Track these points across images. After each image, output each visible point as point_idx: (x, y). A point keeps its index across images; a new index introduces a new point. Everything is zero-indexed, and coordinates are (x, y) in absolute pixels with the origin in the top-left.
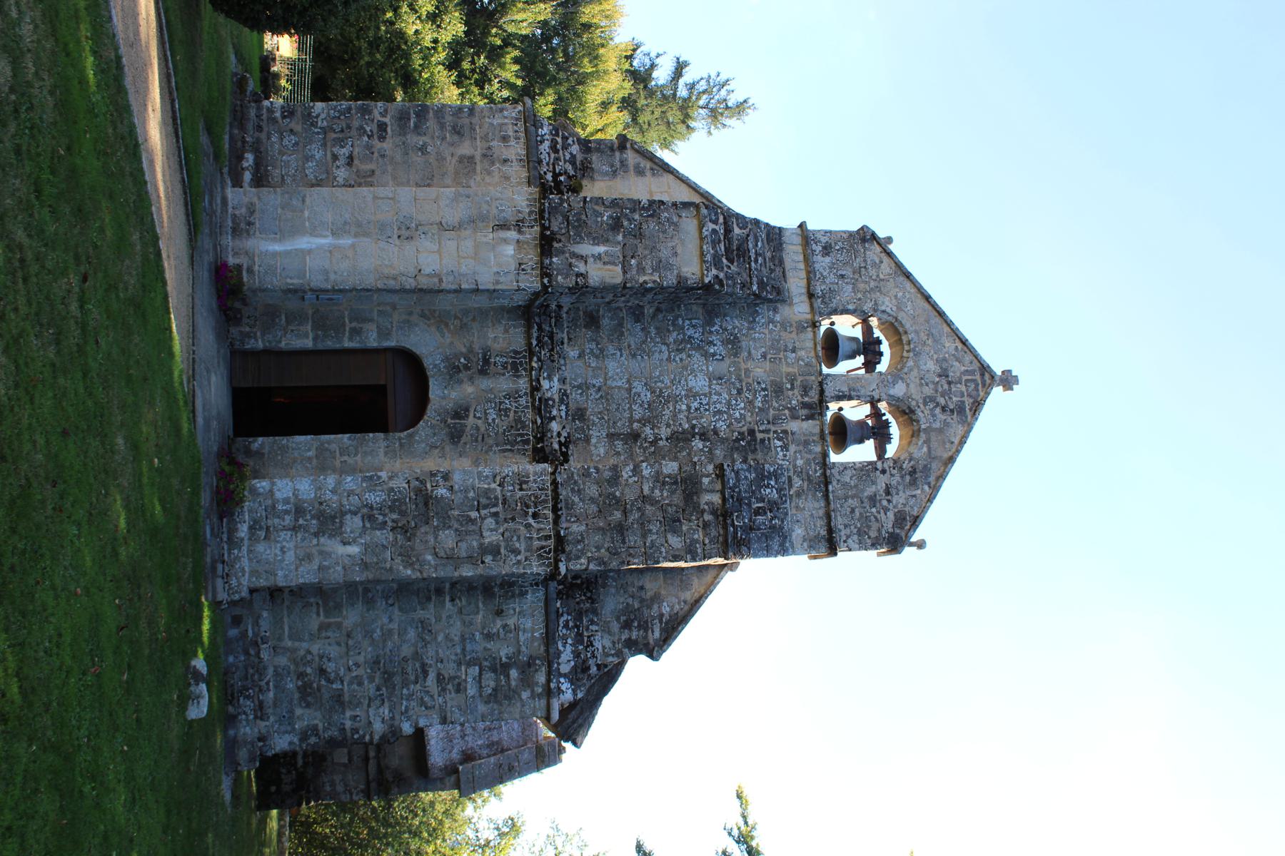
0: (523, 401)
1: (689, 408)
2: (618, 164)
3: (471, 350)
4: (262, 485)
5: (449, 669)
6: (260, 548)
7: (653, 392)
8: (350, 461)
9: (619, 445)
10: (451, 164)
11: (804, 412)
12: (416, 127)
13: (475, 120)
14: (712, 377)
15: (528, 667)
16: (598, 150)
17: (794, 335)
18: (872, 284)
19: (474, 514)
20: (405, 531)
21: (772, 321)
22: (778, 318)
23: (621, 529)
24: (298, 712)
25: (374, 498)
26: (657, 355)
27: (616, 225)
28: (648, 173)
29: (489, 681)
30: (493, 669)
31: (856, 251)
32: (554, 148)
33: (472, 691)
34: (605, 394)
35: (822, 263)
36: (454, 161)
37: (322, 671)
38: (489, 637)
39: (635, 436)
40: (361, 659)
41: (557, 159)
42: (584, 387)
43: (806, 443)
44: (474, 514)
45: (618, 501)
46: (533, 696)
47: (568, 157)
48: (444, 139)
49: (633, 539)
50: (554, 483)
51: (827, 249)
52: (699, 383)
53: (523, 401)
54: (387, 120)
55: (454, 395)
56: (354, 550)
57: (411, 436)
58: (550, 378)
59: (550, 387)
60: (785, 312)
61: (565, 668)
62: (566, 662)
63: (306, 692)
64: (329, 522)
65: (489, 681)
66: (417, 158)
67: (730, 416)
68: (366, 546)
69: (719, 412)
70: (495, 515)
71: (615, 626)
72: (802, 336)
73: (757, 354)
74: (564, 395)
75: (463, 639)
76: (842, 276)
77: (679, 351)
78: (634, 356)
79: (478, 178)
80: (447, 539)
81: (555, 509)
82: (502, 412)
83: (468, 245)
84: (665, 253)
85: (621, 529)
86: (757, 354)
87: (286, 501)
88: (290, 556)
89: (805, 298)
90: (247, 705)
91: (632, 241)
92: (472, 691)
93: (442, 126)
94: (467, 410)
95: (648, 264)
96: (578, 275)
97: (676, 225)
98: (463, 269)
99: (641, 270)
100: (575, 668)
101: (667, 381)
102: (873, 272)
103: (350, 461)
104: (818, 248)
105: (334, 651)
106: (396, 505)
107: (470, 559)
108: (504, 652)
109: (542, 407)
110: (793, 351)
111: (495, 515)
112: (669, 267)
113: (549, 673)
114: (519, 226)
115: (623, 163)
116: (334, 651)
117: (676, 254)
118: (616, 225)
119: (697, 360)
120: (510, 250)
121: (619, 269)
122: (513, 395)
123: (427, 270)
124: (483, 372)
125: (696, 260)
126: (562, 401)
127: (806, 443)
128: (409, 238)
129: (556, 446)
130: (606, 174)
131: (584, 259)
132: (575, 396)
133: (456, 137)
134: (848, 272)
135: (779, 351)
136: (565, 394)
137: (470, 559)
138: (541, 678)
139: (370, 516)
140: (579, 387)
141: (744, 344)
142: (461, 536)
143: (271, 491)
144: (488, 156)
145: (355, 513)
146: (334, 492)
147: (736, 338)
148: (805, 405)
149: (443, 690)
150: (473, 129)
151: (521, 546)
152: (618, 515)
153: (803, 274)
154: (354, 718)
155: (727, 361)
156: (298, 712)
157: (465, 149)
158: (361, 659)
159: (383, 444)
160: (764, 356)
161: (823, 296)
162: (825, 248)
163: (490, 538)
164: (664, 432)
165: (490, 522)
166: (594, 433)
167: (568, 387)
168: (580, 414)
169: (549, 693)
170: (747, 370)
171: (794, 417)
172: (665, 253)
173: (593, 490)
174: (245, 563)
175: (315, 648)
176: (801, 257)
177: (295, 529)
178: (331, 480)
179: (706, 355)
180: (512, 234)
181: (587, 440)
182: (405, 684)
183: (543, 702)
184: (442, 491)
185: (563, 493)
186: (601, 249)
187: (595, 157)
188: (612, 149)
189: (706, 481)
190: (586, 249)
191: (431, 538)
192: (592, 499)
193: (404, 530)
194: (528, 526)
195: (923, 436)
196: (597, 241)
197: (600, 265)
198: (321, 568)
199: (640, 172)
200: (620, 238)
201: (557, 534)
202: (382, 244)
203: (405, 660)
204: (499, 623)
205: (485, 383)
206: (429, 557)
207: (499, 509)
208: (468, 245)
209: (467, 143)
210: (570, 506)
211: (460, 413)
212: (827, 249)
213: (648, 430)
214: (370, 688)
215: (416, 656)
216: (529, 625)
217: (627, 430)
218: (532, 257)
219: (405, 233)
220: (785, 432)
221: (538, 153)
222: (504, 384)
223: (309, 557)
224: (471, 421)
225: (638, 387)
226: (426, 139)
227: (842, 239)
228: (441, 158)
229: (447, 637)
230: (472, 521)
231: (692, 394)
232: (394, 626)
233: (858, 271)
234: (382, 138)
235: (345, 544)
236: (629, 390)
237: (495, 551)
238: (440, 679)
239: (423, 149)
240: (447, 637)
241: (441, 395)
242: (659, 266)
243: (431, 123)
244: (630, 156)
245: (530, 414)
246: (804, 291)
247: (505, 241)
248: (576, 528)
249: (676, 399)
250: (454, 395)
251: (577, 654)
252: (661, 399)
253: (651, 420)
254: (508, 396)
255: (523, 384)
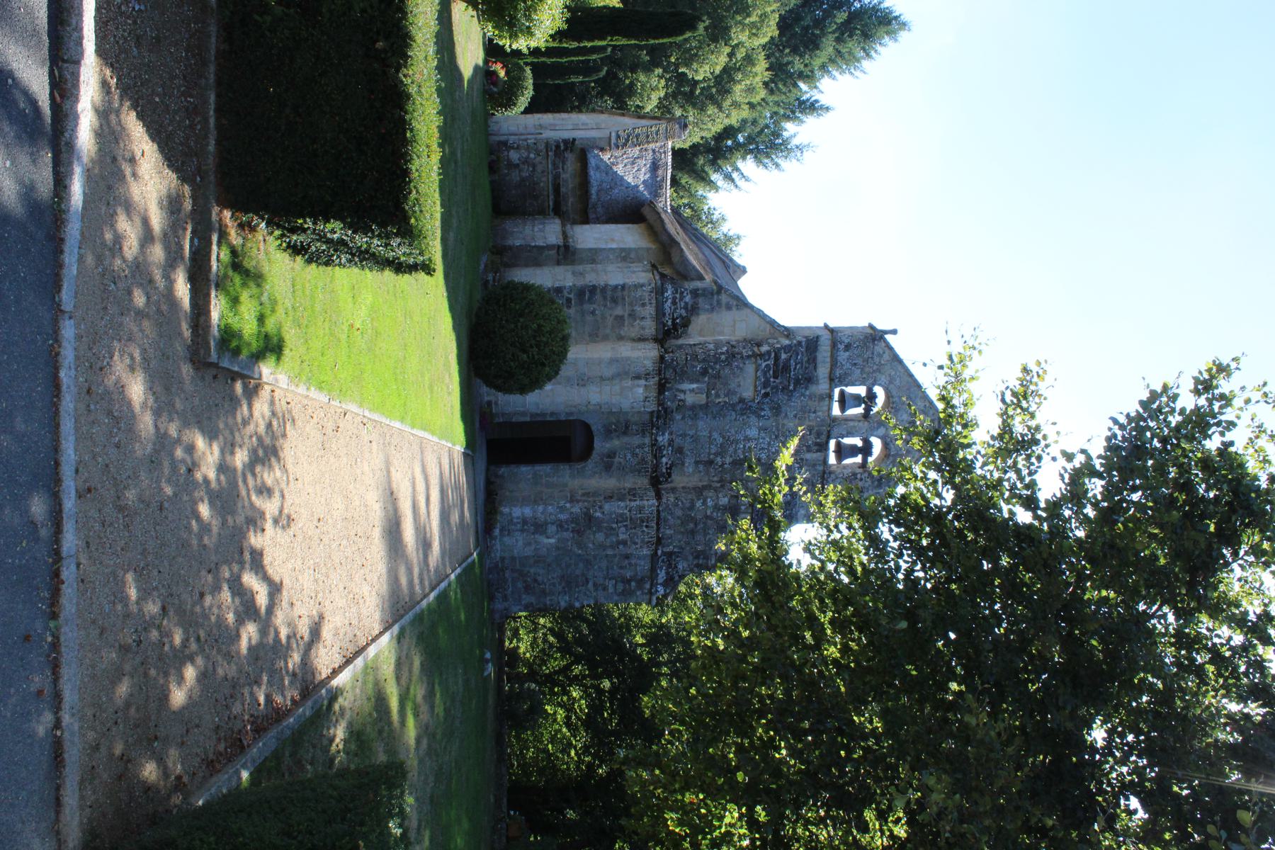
0: (646, 449)
1: (744, 446)
2: (715, 303)
3: (618, 421)
4: (506, 510)
5: (600, 581)
6: (506, 539)
7: (724, 438)
8: (551, 480)
9: (701, 467)
10: (610, 321)
11: (816, 448)
12: (589, 299)
13: (626, 293)
14: (760, 429)
15: (640, 582)
16: (704, 295)
17: (816, 403)
18: (875, 367)
19: (614, 526)
20: (578, 532)
21: (803, 395)
22: (807, 393)
23: (693, 532)
24: (524, 596)
25: (563, 517)
26: (728, 418)
27: (704, 372)
28: (734, 309)
29: (620, 587)
30: (623, 582)
31: (868, 348)
32: (674, 303)
33: (611, 590)
34: (695, 439)
35: (843, 356)
36: (612, 319)
37: (535, 580)
38: (621, 568)
39: (711, 462)
40: (555, 576)
41: (676, 309)
42: (684, 435)
43: (814, 465)
44: (614, 526)
45: (692, 518)
46: (643, 594)
47: (683, 304)
48: (605, 306)
49: (699, 537)
50: (658, 511)
51: (848, 347)
52: (753, 433)
53: (646, 449)
54: (572, 296)
55: (608, 445)
56: (552, 541)
57: (584, 467)
58: (663, 434)
59: (663, 439)
60: (813, 389)
61: (660, 580)
62: (662, 575)
63: (527, 588)
64: (539, 527)
65: (620, 587)
66: (589, 318)
67: (769, 450)
68: (559, 539)
69: (763, 449)
70: (626, 526)
71: (691, 558)
72: (822, 403)
73: (791, 415)
74: (671, 442)
75: (608, 569)
76: (855, 364)
77: (742, 414)
78: (715, 418)
79: (626, 329)
80: (600, 537)
81: (658, 524)
82: (634, 455)
83: (617, 388)
84: (733, 386)
85: (693, 532)
86: (791, 415)
87: (518, 518)
88: (520, 543)
89: (827, 380)
90: (499, 595)
91: (713, 380)
92: (611, 590)
93: (605, 298)
94: (615, 454)
95: (722, 393)
96: (680, 400)
97: (741, 369)
98: (614, 401)
99: (717, 396)
100: (666, 581)
101: (733, 432)
102: (877, 360)
103: (551, 480)
104: (841, 347)
105: (541, 572)
106: (574, 520)
107: (612, 547)
108: (628, 574)
109: (657, 451)
110: (815, 412)
111: (626, 526)
112: (735, 393)
113: (652, 585)
114: (647, 376)
115: (719, 302)
116: (541, 572)
117: (739, 386)
118: (704, 372)
119: (753, 419)
120: (641, 390)
121: (704, 395)
122: (641, 446)
123: (593, 402)
124: (625, 433)
125: (752, 388)
126: (669, 445)
127: (814, 465)
128: (584, 385)
129: (664, 471)
130: (708, 310)
131: (684, 392)
132: (678, 441)
133: (613, 305)
134: (860, 361)
135: (804, 412)
136: (672, 440)
137: (612, 547)
138: (648, 586)
139: (561, 525)
140: (681, 435)
141: (783, 409)
142: (607, 536)
143: (510, 514)
144: (632, 315)
145: (553, 524)
146: (542, 513)
147: (779, 405)
148: (816, 444)
149: (596, 590)
150: (624, 299)
151: (638, 541)
152: (692, 525)
153: (828, 365)
154: (551, 600)
155: (772, 419)
156: (524, 596)
157: (619, 311)
158: (555, 576)
159: (568, 472)
160: (795, 416)
161: (840, 377)
162: (846, 346)
163: (622, 537)
164: (728, 460)
165: (623, 529)
166: (687, 460)
167: (674, 437)
168: (680, 450)
169: (651, 593)
170: (783, 425)
171: (809, 451)
172: (733, 386)
173: (679, 513)
174: (498, 547)
175: (532, 571)
176: (829, 354)
177: (522, 531)
178: (541, 508)
179: (759, 417)
180: (643, 382)
181: (683, 464)
182: (577, 586)
183: (648, 597)
184: (598, 514)
185: (663, 514)
186: (695, 386)
187: (700, 300)
188: (712, 294)
189: (743, 508)
190: (687, 386)
191: (592, 537)
192: (678, 518)
193: (578, 532)
194: (643, 531)
195: (891, 458)
196: (692, 382)
197: (693, 394)
198: (536, 549)
199: (729, 308)
200: (706, 379)
201: (658, 537)
202: (568, 388)
203: (578, 576)
204: (626, 562)
205: (626, 439)
206: (591, 545)
207: (628, 523)
208: (617, 388)
209: (619, 308)
210: (666, 520)
211: (612, 454)
212: (848, 347)
213: (719, 459)
214: (560, 588)
215: (583, 575)
216: (642, 563)
217: (706, 459)
218: (653, 394)
219: (580, 382)
220: (802, 459)
221: (663, 309)
222: (636, 440)
223: (530, 544)
224: (617, 460)
225: (715, 435)
226: (595, 306)
227: (859, 340)
228: (604, 317)
229: (599, 567)
230: (614, 529)
231: (747, 439)
232: (573, 562)
233: (867, 361)
234: (569, 307)
235: (548, 538)
236: (710, 437)
237: (624, 543)
238: (595, 585)
239: (593, 313)
240: (599, 567)
241: (600, 446)
242: (729, 393)
243: (598, 297)
244: (724, 298)
245: (650, 457)
246: (827, 375)
247: (638, 386)
248: (668, 532)
249: (737, 442)
250: (608, 445)
251: (667, 573)
252: (728, 441)
253: (722, 452)
254: (639, 446)
255: (647, 440)
